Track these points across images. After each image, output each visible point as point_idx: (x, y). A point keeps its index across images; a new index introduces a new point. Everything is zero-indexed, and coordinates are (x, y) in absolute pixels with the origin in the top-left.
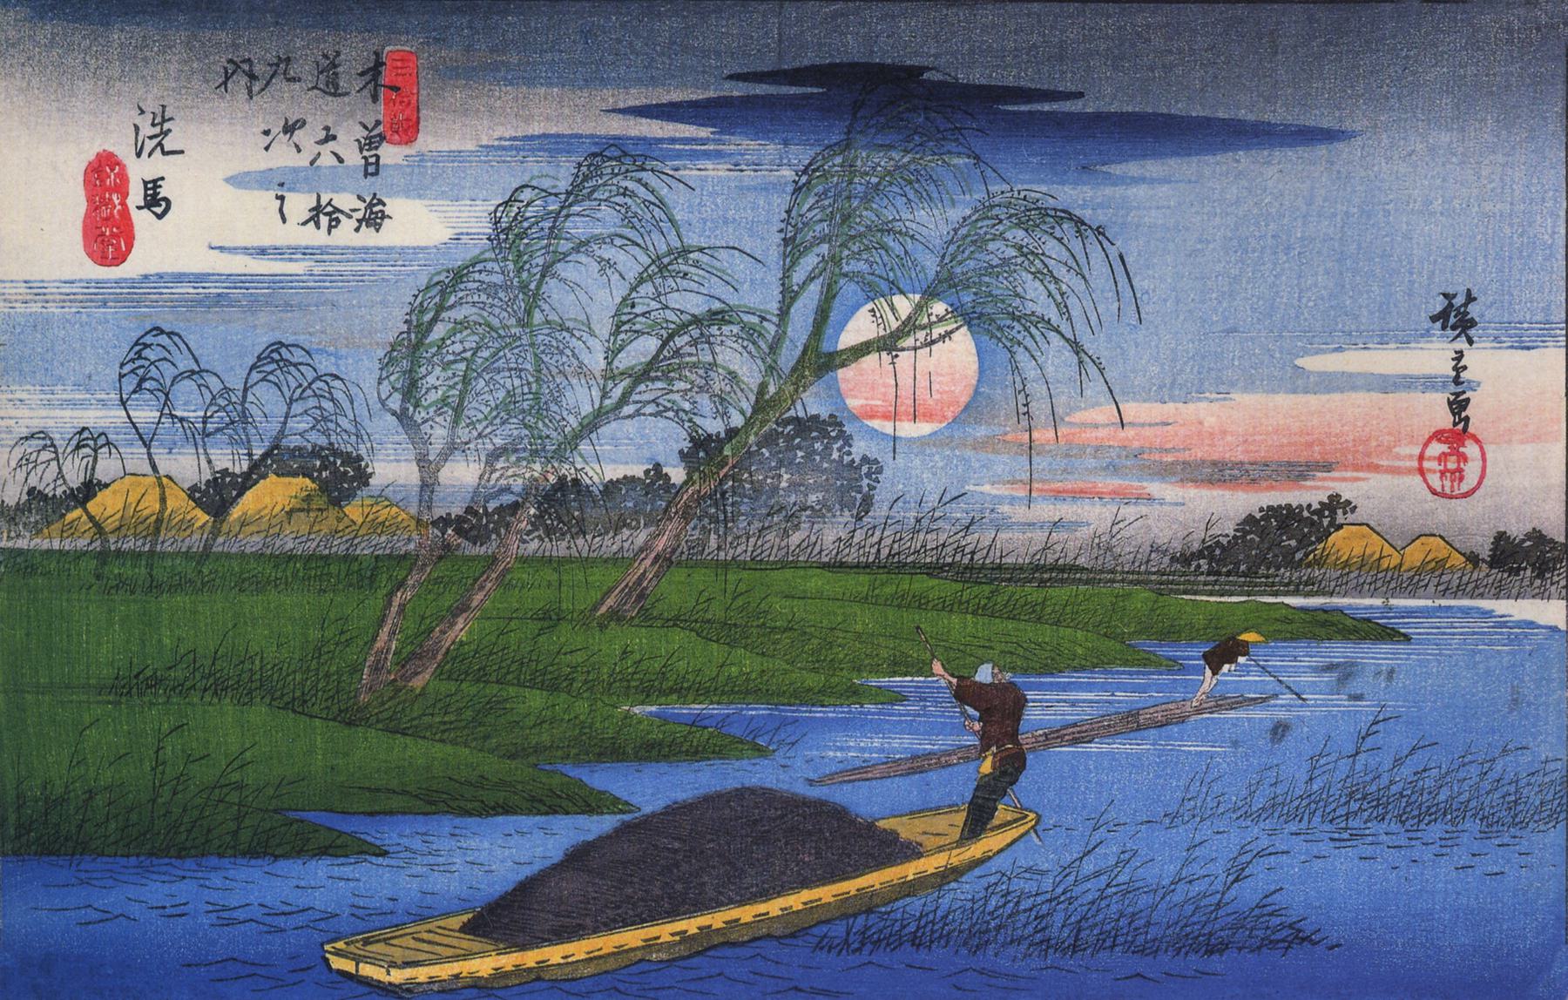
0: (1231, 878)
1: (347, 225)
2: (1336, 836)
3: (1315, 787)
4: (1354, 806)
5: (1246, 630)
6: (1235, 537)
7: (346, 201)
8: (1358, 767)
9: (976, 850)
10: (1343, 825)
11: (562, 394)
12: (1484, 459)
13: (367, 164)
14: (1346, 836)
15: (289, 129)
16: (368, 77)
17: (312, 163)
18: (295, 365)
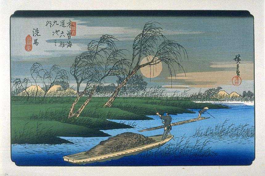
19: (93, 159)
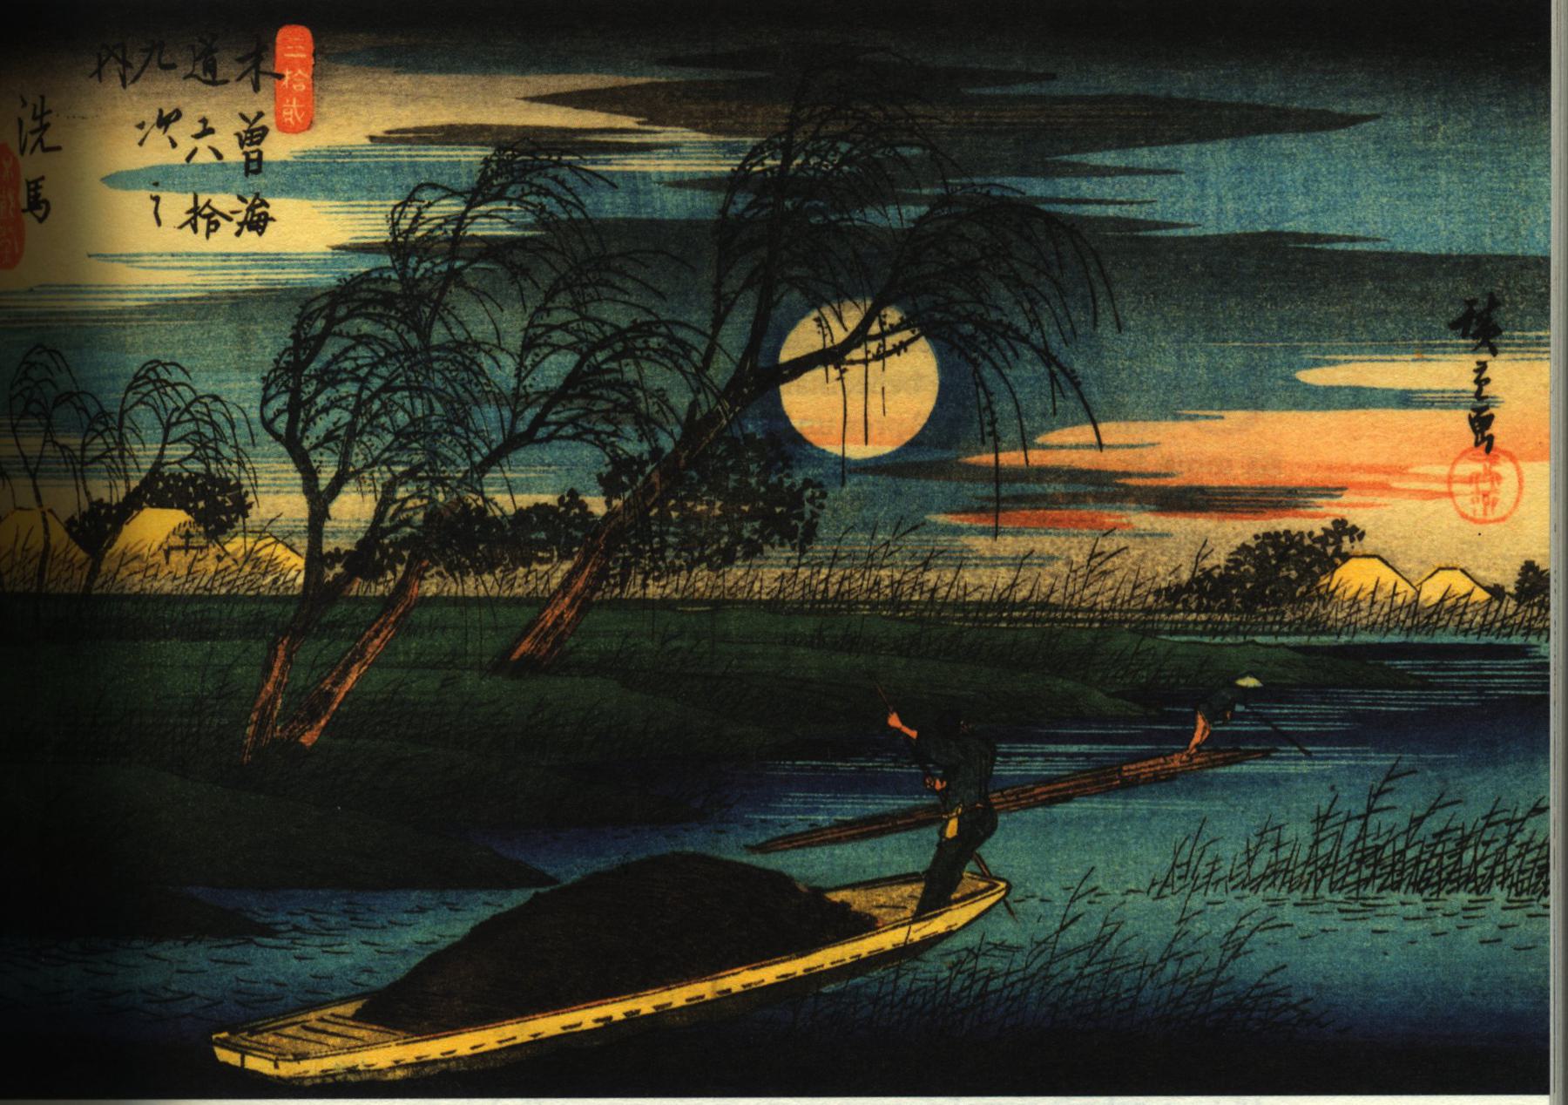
0: (1229, 953)
1: (227, 229)
2: (1345, 906)
3: (1321, 852)
4: (1366, 873)
5: (1243, 676)
6: (1227, 568)
7: (225, 202)
8: (1371, 828)
9: (938, 925)
10: (1354, 894)
11: (468, 414)
12: (1521, 481)
13: (248, 160)
14: (1357, 906)
15: (164, 122)
16: (248, 64)
17: (189, 159)
18: (173, 386)
19: (630, 1005)
